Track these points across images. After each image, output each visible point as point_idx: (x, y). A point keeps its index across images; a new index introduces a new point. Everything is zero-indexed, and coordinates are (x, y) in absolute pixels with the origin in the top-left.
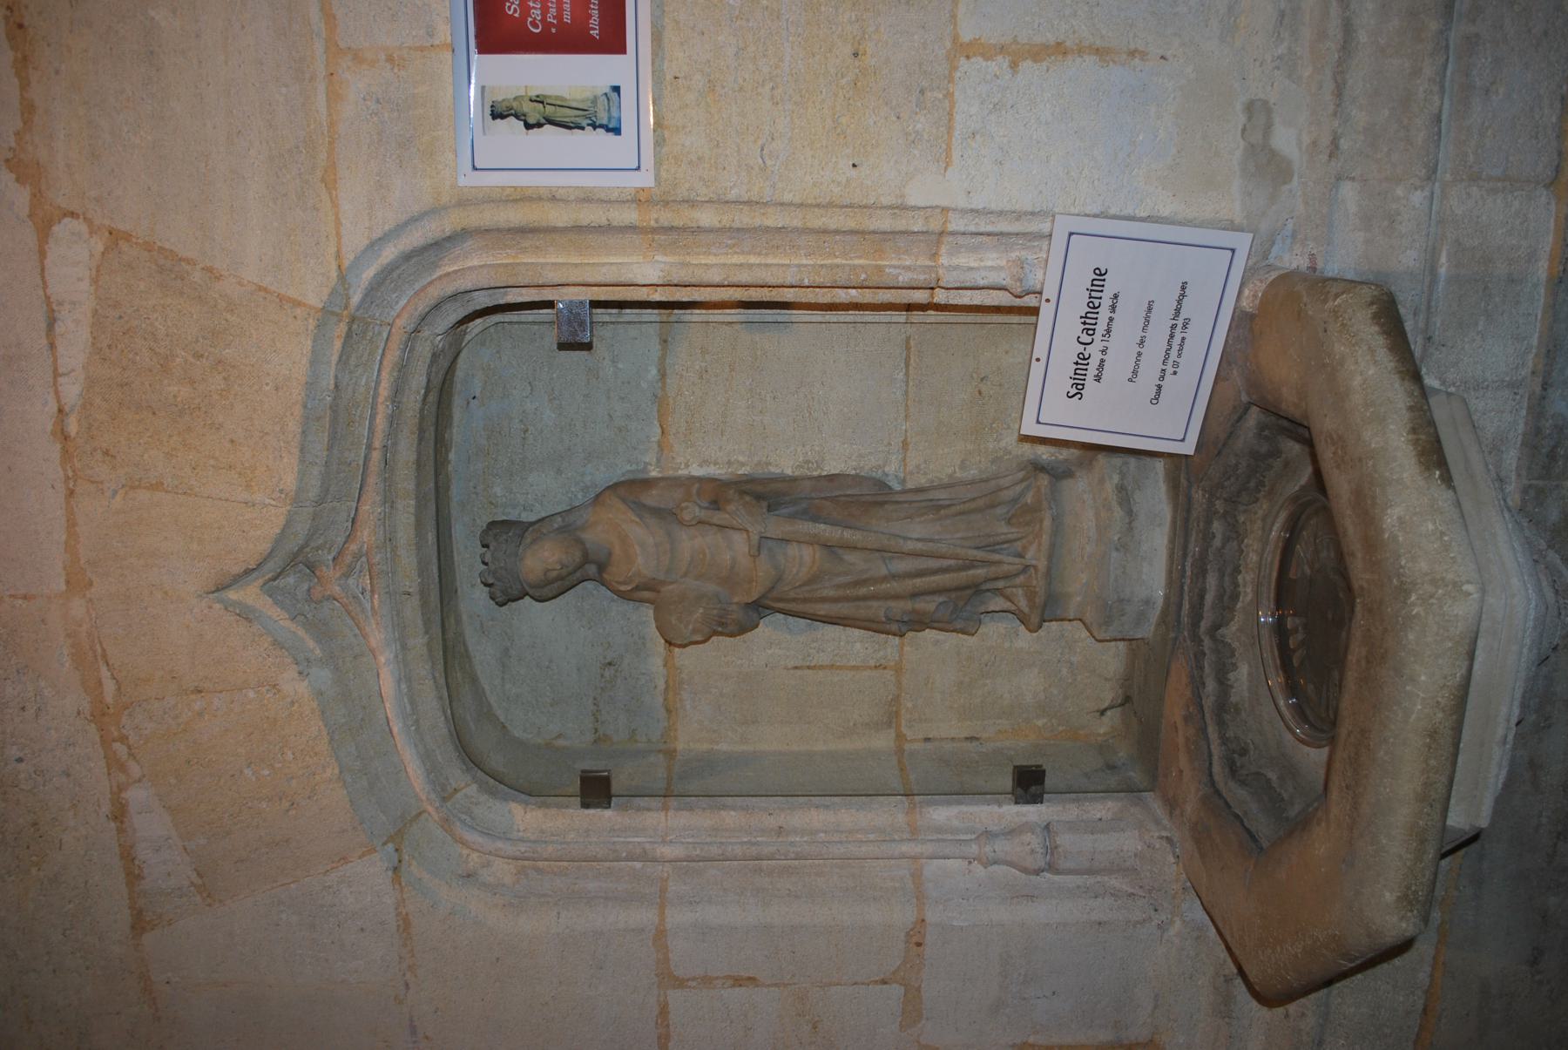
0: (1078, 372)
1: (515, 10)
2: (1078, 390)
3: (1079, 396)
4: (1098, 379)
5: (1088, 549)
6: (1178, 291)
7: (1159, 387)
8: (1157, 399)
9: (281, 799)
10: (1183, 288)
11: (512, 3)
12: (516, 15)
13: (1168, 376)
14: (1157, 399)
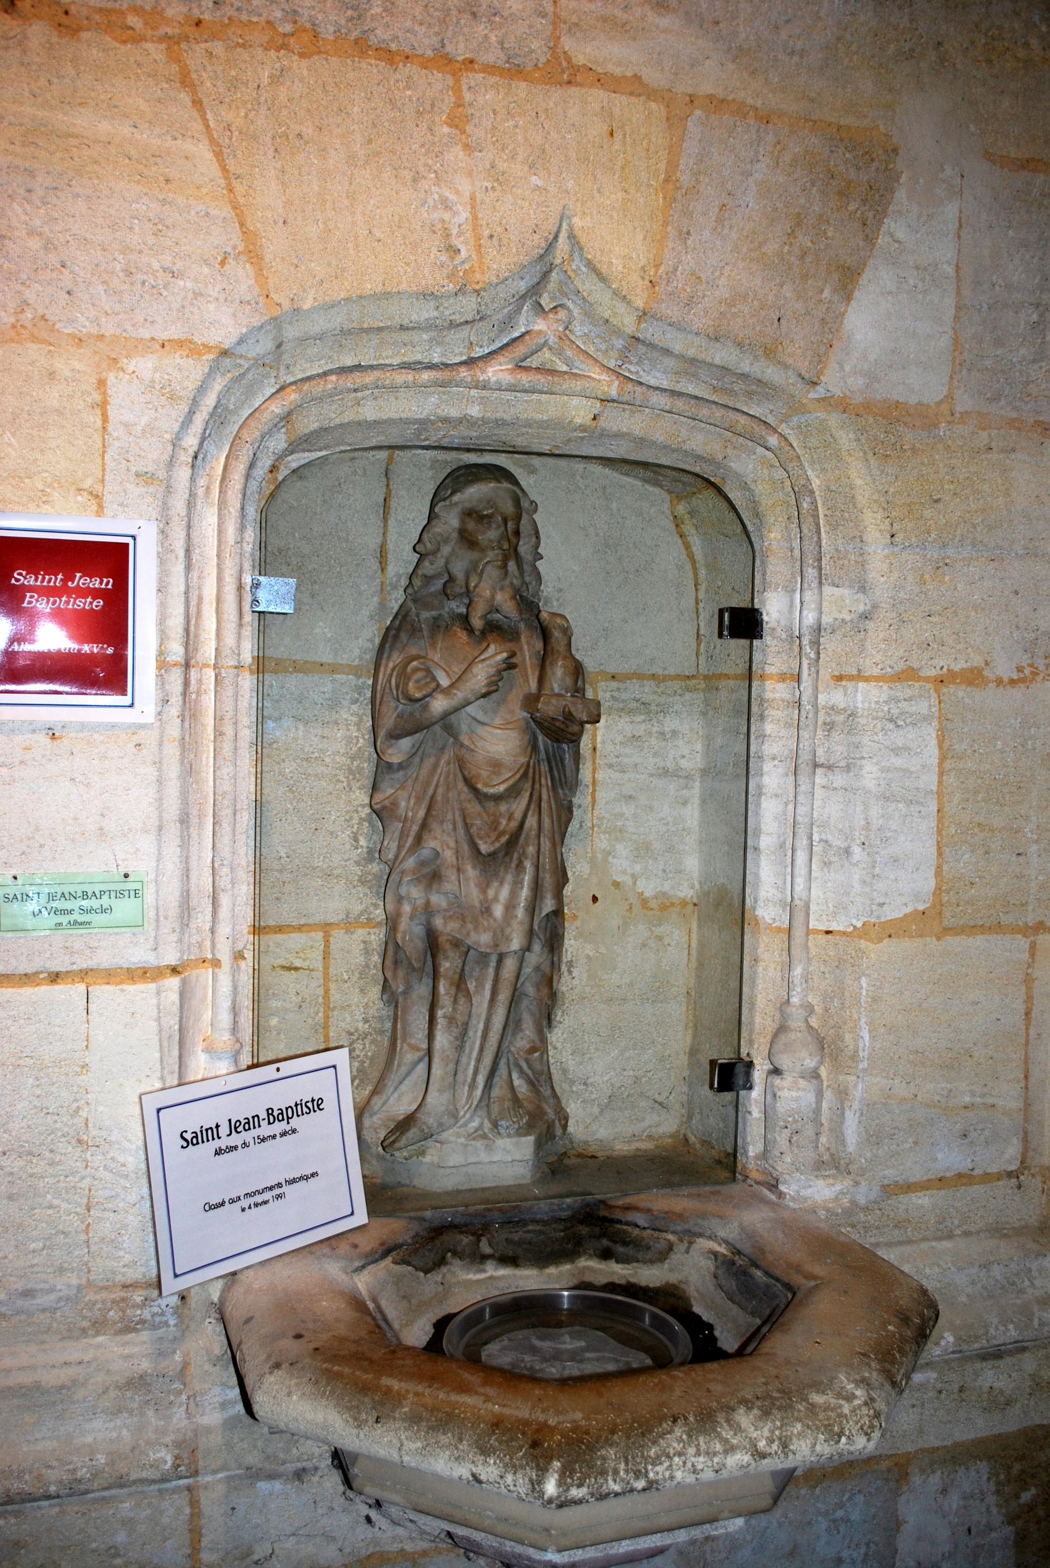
0: (210, 1132)
1: (17, 580)
2: (191, 1140)
3: (185, 1144)
4: (218, 1152)
5: (13, 1521)
6: (308, 1172)
7: (222, 1204)
8: (210, 1208)
9: (675, 1421)
10: (313, 1175)
11: (25, 578)
12: (13, 581)
13: (237, 1206)
14: (210, 1208)
